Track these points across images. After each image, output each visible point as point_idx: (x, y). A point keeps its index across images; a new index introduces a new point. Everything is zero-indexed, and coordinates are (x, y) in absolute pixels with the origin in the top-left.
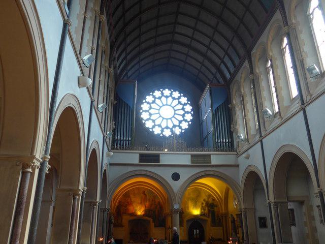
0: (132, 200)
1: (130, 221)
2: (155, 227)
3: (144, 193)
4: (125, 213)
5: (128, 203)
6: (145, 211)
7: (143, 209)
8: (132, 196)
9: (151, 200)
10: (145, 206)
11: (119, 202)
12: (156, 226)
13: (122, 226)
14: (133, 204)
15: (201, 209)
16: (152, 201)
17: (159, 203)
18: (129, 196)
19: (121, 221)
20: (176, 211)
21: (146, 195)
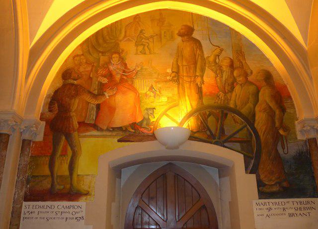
0: (131, 66)
1: (117, 171)
2: (263, 195)
3: (188, 33)
4: (95, 126)
5: (110, 76)
6: (203, 114)
7: (187, 105)
8: (129, 48)
9: (225, 64)
10: (199, 91)
11: (66, 74)
12: (264, 193)
13: (72, 194)
14: (137, 83)
15: (195, 96)
16: (232, 66)
17: (268, 77)
18: (116, 50)
19: (72, 167)
20: (121, 76)
21: (198, 43)
